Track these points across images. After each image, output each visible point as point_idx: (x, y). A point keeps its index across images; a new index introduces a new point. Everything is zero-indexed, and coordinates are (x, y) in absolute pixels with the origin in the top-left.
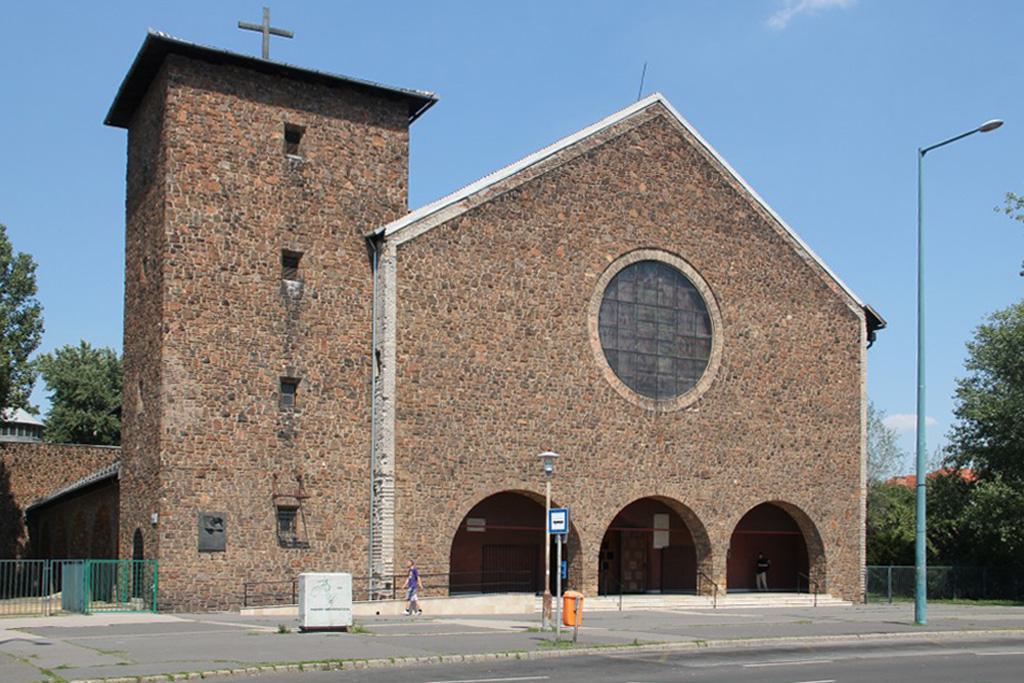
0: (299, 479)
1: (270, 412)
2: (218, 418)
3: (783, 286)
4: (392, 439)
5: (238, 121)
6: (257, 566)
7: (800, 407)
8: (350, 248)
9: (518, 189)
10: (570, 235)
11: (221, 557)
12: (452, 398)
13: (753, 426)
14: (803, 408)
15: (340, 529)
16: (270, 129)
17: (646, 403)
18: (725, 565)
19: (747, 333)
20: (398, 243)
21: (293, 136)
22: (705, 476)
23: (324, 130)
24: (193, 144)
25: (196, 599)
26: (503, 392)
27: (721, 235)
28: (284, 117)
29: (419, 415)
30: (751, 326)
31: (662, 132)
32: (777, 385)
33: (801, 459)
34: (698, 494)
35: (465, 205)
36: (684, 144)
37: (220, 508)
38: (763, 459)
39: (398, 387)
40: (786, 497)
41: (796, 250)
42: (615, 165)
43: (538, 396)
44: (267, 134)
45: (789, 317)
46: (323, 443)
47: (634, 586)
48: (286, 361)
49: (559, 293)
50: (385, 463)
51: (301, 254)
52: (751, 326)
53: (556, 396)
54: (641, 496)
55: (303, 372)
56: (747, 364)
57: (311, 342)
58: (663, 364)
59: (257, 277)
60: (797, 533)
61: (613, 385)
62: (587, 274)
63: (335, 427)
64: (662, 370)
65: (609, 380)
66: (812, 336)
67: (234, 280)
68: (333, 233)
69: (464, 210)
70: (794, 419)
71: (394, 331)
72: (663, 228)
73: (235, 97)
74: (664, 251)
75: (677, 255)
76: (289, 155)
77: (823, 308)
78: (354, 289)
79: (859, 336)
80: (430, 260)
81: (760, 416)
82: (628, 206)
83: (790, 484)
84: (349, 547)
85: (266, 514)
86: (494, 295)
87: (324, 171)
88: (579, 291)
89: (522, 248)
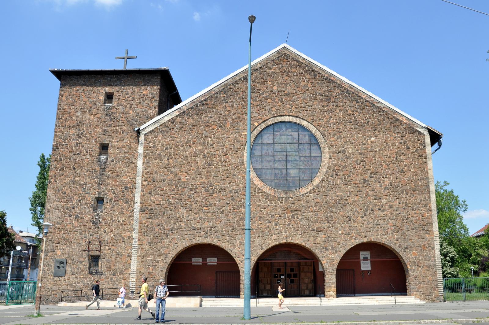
0: (100, 242)
1: (89, 213)
2: (67, 217)
3: (367, 123)
4: (138, 221)
5: (86, 95)
6: (78, 283)
7: (384, 187)
8: (130, 138)
9: (205, 100)
10: (234, 116)
11: (63, 279)
12: (168, 200)
13: (350, 200)
14: (385, 188)
15: (119, 265)
16: (98, 96)
17: (280, 193)
18: (335, 280)
19: (344, 150)
20: (145, 133)
21: (109, 97)
22: (319, 230)
23: (122, 92)
24: (67, 107)
25: (51, 298)
26: (195, 195)
27: (325, 103)
28: (105, 90)
29: (151, 209)
30: (346, 147)
31: (286, 60)
32: (366, 176)
33: (386, 216)
34: (315, 240)
35: (178, 111)
36: (299, 64)
37: (65, 257)
38: (359, 218)
39: (142, 197)
40: (378, 239)
41: (375, 104)
42: (259, 80)
43: (215, 195)
44: (97, 98)
45: (373, 139)
46: (112, 225)
47: (307, 292)
48: (98, 190)
49: (227, 145)
50: (134, 233)
51: (108, 144)
52: (346, 147)
53: (225, 194)
54: (277, 243)
55: (105, 194)
56: (345, 167)
57: (110, 181)
58: (293, 172)
59: (88, 156)
60: (398, 260)
61: (258, 186)
62: (243, 133)
63: (118, 218)
64: (292, 176)
65: (256, 184)
66: (389, 148)
67: (79, 158)
68: (123, 133)
69: (178, 113)
70: (380, 194)
71: (141, 172)
72: (288, 105)
73: (85, 87)
74: (289, 116)
75: (297, 117)
76: (105, 105)
77: (397, 131)
78: (131, 156)
79: (425, 143)
80: (160, 138)
81: (356, 195)
82: (267, 98)
83: (379, 231)
84: (122, 274)
85: (85, 259)
86: (192, 150)
87: (121, 109)
88: (238, 142)
89: (207, 126)
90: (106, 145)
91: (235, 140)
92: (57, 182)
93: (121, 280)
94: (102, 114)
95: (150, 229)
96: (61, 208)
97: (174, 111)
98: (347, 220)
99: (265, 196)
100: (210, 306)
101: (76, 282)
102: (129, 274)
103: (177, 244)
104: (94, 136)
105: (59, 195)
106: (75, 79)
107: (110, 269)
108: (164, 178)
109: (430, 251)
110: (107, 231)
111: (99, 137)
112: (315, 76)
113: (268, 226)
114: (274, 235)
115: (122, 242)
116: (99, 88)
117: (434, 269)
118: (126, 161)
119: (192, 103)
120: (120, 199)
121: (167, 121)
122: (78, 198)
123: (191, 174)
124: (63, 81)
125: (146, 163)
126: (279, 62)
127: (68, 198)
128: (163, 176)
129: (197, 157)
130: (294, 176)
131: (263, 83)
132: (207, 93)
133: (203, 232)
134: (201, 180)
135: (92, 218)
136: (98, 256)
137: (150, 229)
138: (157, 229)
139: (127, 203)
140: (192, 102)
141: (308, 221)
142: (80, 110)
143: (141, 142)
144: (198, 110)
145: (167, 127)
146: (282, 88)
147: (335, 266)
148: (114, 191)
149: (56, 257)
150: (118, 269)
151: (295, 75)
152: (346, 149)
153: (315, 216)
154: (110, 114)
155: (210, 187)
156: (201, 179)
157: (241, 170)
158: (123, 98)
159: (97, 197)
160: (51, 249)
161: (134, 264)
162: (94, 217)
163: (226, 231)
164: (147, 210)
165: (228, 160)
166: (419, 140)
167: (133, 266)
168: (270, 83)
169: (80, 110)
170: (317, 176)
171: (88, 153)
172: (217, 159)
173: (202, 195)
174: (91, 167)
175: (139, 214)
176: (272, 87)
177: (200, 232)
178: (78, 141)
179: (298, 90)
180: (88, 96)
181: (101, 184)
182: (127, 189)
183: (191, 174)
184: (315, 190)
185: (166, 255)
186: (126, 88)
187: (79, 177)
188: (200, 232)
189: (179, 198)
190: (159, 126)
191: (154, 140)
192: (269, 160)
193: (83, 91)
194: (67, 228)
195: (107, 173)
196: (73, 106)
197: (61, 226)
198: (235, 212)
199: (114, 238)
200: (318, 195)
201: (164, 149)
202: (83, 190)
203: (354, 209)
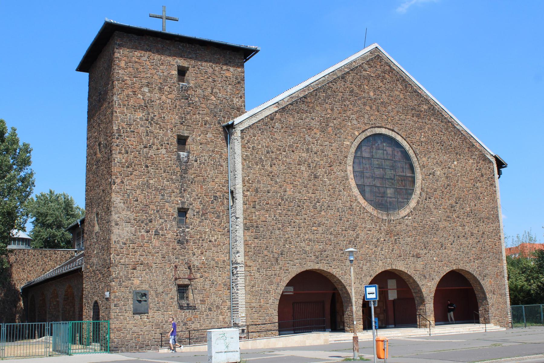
0: (189, 268)
1: (172, 229)
5: (152, 65)
9: (305, 97)
11: (146, 317)
12: (275, 217)
13: (441, 226)
14: (468, 214)
18: (433, 309)
19: (434, 172)
21: (182, 72)
22: (418, 256)
23: (199, 69)
24: (128, 78)
27: (415, 119)
28: (177, 62)
32: (452, 201)
33: (469, 244)
35: (277, 106)
36: (391, 70)
38: (449, 245)
39: (244, 211)
45: (455, 163)
50: (239, 256)
51: (188, 137)
54: (383, 270)
55: (191, 205)
59: (164, 151)
63: (209, 236)
68: (205, 124)
69: (277, 109)
74: (386, 128)
75: (393, 130)
76: (180, 83)
78: (218, 156)
81: (445, 220)
82: (365, 104)
85: (171, 289)
86: (295, 156)
90: (183, 138)
91: (338, 150)
92: (125, 183)
93: (219, 317)
94: (177, 95)
95: (258, 252)
96: (134, 220)
97: (271, 105)
98: (440, 246)
99: (370, 217)
100: (334, 342)
101: (162, 320)
102: (227, 307)
103: (288, 270)
104: (168, 123)
105: (130, 202)
106: (136, 39)
107: (204, 303)
108: (268, 188)
109: (501, 279)
110: (196, 254)
111: (175, 127)
112: (406, 87)
113: (375, 251)
114: (380, 261)
115: (216, 268)
116: (169, 59)
117: (505, 297)
118: (213, 162)
119: (290, 98)
120: (209, 212)
121: (265, 117)
122: (155, 208)
123: (296, 186)
124: (119, 40)
125: (246, 168)
126: (374, 64)
127: (143, 208)
128: (267, 186)
129: (301, 166)
130: (391, 196)
131: (360, 86)
132: (305, 88)
133: (314, 257)
134: (308, 194)
135: (177, 236)
136: (187, 286)
137: (258, 252)
138: (265, 252)
139: (218, 217)
140: (291, 96)
141: (409, 246)
142: (147, 85)
143: (237, 140)
144: (298, 109)
145: (266, 124)
146: (378, 95)
147: (433, 295)
148: (201, 201)
149: (133, 288)
150: (213, 302)
151: (389, 82)
152: (435, 171)
153: (414, 241)
154: (186, 96)
155: (318, 204)
156: (307, 192)
157: (346, 185)
158: (202, 78)
159: (181, 207)
160: (126, 277)
161: (241, 295)
162: (179, 234)
163: (336, 255)
164: (253, 228)
165: (334, 173)
166: (489, 168)
167: (241, 298)
168: (367, 87)
169: (147, 85)
170: (413, 198)
171: (163, 147)
172: (322, 170)
173: (310, 213)
174: (169, 167)
175: (243, 232)
176: (368, 93)
177: (310, 257)
178: (148, 129)
179: (392, 100)
180: (155, 67)
181: (184, 191)
182: (217, 199)
183: (296, 186)
184: (412, 213)
185: (278, 284)
186: (204, 64)
187: (154, 179)
188: (310, 257)
189: (287, 215)
190: (257, 122)
191: (252, 139)
192: (368, 176)
193: (148, 59)
194: (144, 249)
195: (190, 176)
196: (137, 79)
197: (136, 245)
198: (344, 234)
199: (206, 262)
200: (415, 218)
201: (265, 153)
202: (162, 197)
203: (445, 235)
